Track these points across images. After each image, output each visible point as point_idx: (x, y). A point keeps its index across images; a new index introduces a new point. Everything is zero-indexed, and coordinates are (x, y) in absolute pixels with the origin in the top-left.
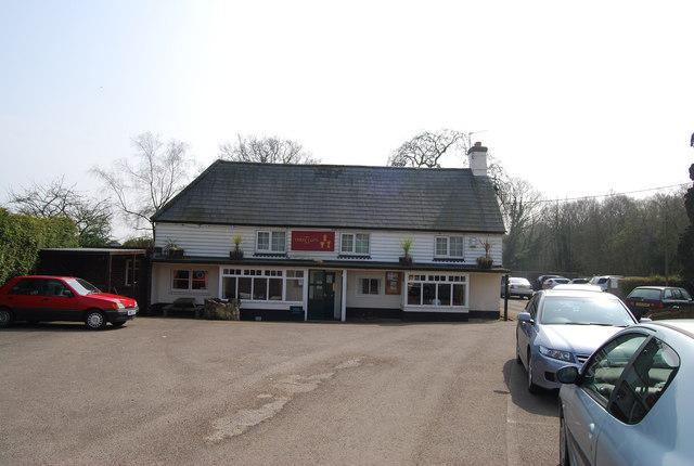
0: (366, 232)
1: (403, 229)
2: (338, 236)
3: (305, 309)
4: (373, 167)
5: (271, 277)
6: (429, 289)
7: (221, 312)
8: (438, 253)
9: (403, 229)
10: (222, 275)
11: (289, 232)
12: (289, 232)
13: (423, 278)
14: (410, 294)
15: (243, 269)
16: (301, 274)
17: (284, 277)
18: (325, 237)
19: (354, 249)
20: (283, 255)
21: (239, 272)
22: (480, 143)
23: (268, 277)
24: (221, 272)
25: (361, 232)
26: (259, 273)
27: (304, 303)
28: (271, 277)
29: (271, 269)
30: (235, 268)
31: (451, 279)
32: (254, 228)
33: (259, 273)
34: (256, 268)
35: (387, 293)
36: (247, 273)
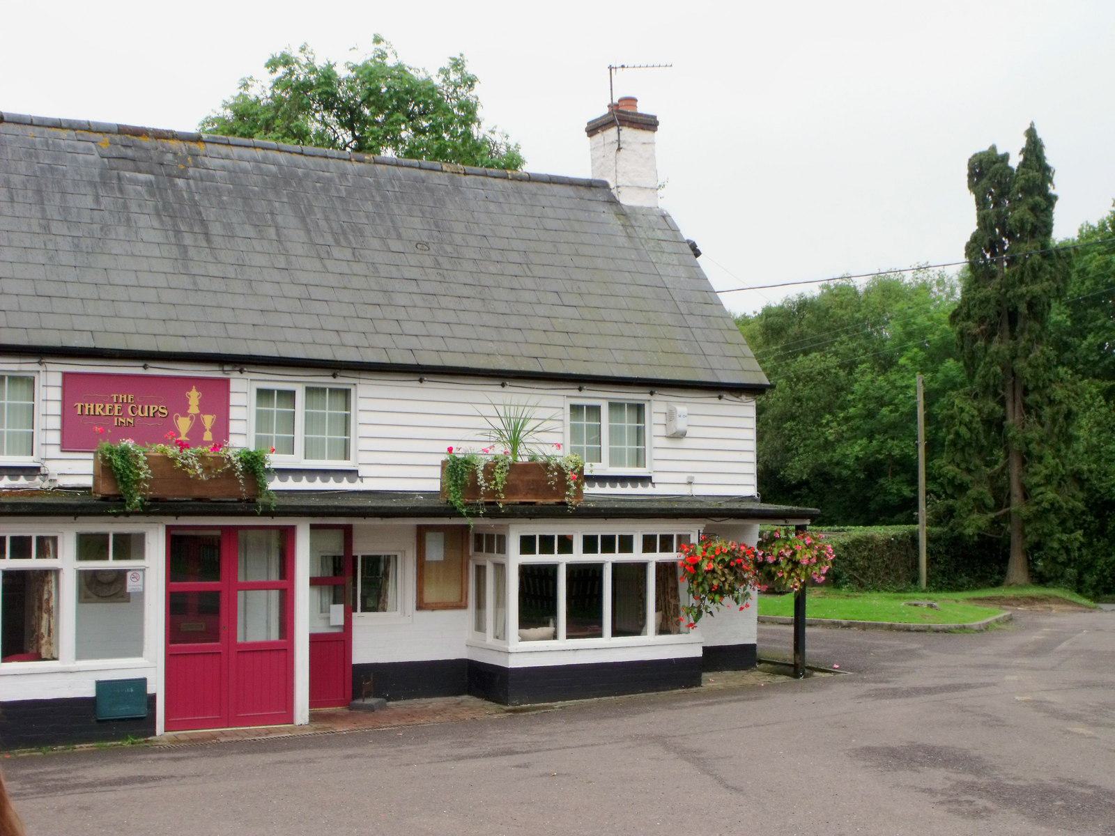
0: (342, 381)
1: (256, 380)
2: (243, 391)
3: (157, 686)
6: (585, 581)
9: (256, 380)
10: (515, 559)
11: (49, 381)
12: (49, 381)
15: (578, 531)
18: (194, 397)
20: (31, 471)
22: (632, 101)
24: (514, 544)
25: (323, 380)
26: (626, 544)
27: (149, 665)
28: (618, 557)
33: (626, 544)
34: (616, 529)
35: (421, 606)
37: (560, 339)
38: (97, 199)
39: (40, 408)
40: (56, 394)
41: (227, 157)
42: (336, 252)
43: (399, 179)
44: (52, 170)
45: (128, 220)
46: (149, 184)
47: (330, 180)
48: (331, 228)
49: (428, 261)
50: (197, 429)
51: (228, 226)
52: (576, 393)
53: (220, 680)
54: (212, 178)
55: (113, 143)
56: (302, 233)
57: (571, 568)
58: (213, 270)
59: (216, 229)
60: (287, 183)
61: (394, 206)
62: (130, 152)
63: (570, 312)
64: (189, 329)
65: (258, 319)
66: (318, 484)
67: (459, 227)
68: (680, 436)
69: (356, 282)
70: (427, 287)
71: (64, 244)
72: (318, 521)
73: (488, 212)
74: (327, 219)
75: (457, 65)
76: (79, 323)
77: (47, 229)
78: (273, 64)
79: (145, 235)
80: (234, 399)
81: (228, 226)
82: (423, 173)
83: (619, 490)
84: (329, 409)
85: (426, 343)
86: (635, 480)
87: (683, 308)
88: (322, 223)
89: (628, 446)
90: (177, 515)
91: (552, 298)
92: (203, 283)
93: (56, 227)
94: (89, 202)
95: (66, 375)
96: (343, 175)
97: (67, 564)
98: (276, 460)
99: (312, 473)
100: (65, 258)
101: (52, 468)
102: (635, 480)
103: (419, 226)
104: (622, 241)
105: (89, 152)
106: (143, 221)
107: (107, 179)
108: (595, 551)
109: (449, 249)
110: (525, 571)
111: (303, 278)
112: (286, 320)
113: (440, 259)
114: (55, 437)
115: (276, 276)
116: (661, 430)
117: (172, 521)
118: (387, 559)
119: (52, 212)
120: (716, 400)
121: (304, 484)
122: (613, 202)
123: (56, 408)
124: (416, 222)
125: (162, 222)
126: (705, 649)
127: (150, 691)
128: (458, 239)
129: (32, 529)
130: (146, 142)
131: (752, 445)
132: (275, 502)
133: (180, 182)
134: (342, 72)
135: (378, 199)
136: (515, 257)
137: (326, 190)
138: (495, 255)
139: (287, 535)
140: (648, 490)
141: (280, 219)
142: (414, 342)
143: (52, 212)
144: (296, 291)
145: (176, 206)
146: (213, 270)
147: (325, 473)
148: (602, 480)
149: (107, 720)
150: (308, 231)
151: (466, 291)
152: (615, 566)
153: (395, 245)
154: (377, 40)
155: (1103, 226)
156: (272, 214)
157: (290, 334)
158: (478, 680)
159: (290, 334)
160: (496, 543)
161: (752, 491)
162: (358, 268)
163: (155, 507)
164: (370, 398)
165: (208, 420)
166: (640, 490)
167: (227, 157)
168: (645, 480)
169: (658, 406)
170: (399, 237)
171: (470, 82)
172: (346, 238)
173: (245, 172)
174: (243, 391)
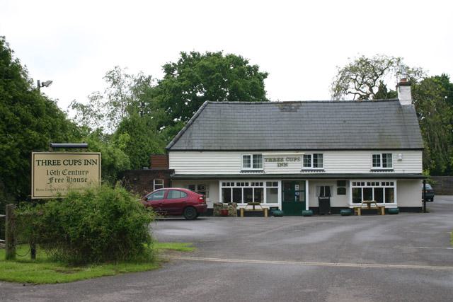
4: (323, 102)
5: (255, 187)
6: (368, 192)
8: (374, 165)
10: (221, 187)
13: (363, 184)
14: (354, 195)
16: (276, 184)
17: (265, 187)
19: (381, 165)
21: (363, 184)
23: (253, 187)
26: (378, 184)
27: (279, 204)
28: (255, 187)
31: (383, 184)
32: (370, 152)
33: (247, 184)
34: (375, 181)
68: (400, 160)
86: (389, 170)
108: (326, 187)
110: (223, 189)
121: (247, 173)
131: (421, 159)
134: (224, 55)
140: (393, 172)
149: (272, 212)
152: (386, 189)
155: (58, 110)
166: (390, 172)
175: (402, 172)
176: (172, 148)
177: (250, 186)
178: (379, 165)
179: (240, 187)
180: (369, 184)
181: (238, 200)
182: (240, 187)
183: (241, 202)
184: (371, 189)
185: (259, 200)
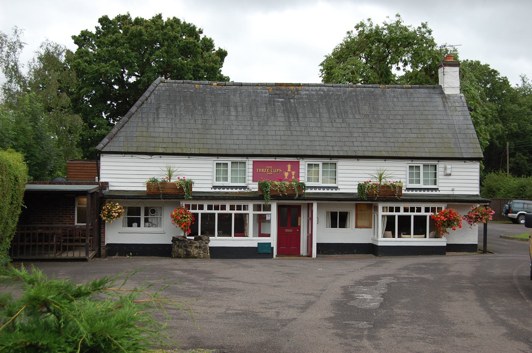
0: (333, 161)
2: (303, 164)
3: (274, 245)
6: (404, 221)
7: (194, 251)
8: (217, 179)
10: (381, 213)
11: (250, 163)
12: (250, 163)
13: (201, 207)
15: (402, 206)
16: (268, 208)
17: (251, 212)
18: (289, 166)
20: (245, 187)
23: (233, 212)
26: (419, 210)
27: (273, 240)
28: (220, 211)
29: (236, 203)
30: (394, 205)
31: (427, 210)
33: (419, 210)
34: (416, 205)
36: (406, 210)
37: (407, 145)
38: (267, 109)
39: (247, 170)
40: (251, 166)
41: (308, 90)
42: (337, 121)
43: (364, 92)
44: (255, 100)
45: (275, 114)
46: (282, 102)
47: (340, 95)
48: (337, 112)
49: (367, 121)
50: (290, 175)
51: (305, 114)
52: (411, 162)
53: (289, 245)
54: (302, 98)
55: (273, 89)
56: (327, 114)
57: (399, 217)
58: (298, 129)
59: (301, 115)
60: (326, 98)
61: (360, 102)
62: (278, 92)
63: (413, 135)
64: (288, 148)
65: (309, 143)
66: (326, 191)
67: (381, 108)
69: (342, 130)
70: (365, 130)
71: (256, 124)
72: (319, 202)
73: (393, 102)
74: (337, 109)
75: (424, 26)
76: (257, 147)
77: (251, 119)
78: (357, 27)
79: (279, 119)
80: (301, 167)
81: (305, 114)
82: (373, 89)
83: (430, 192)
84: (329, 169)
85: (360, 148)
86: (432, 189)
87: (458, 131)
88: (335, 111)
89: (431, 178)
90: (279, 200)
91: (409, 131)
92: (294, 133)
93: (255, 118)
94: (264, 110)
95: (253, 161)
96: (345, 93)
97: (251, 212)
98: (308, 184)
99: (324, 188)
100: (256, 128)
101: (250, 186)
102: (432, 189)
103: (367, 109)
104: (441, 108)
105: (266, 93)
106: (279, 114)
107: (271, 102)
109: (376, 116)
111: (325, 129)
112: (318, 143)
113: (372, 120)
114: (251, 178)
115: (317, 129)
116: (443, 173)
117: (278, 202)
118: (347, 213)
119: (254, 113)
120: (464, 163)
121: (322, 191)
122: (442, 93)
123: (251, 170)
124: (366, 107)
125: (285, 114)
126: (447, 244)
127: (272, 246)
128: (380, 112)
129: (242, 203)
130: (283, 88)
131: (478, 174)
132: (306, 196)
133: (292, 100)
135: (355, 100)
136: (399, 117)
137: (338, 99)
138: (391, 117)
139: (310, 206)
141: (321, 110)
142: (356, 148)
143: (254, 113)
144: (322, 134)
145: (290, 109)
146: (298, 129)
147: (328, 188)
148: (311, 188)
149: (261, 253)
150: (329, 114)
151: (377, 130)
152: (202, 214)
153: (357, 116)
154: (398, 15)
156: (319, 109)
157: (318, 148)
158: (370, 249)
159: (318, 148)
160: (376, 208)
161: (478, 193)
162: (343, 125)
163: (275, 197)
164: (342, 166)
165: (293, 173)
166: (434, 192)
167: (308, 90)
168: (436, 189)
169: (441, 166)
170: (360, 113)
171: (430, 32)
172: (342, 115)
173: (313, 95)
174: (303, 164)
175: (451, 193)
176: (103, 150)
177: (228, 211)
178: (226, 179)
179: (213, 211)
180: (210, 207)
181: (209, 231)
182: (213, 211)
183: (213, 235)
184: (394, 216)
185: (241, 231)
